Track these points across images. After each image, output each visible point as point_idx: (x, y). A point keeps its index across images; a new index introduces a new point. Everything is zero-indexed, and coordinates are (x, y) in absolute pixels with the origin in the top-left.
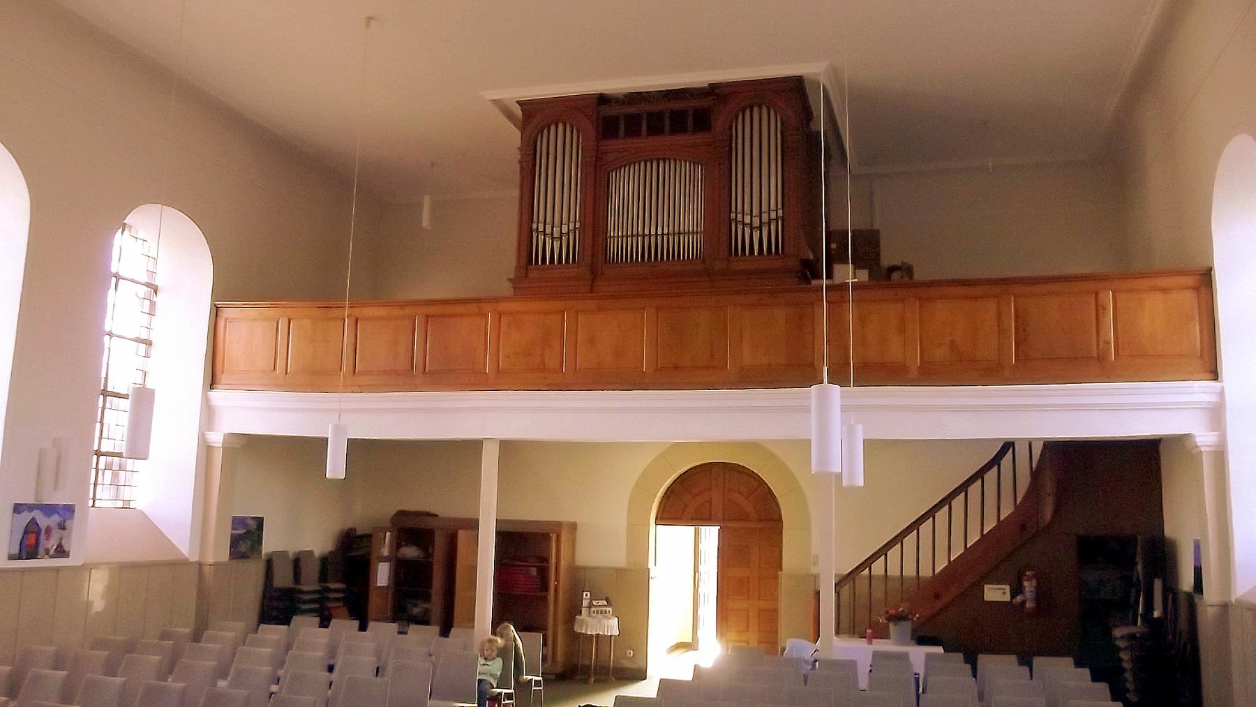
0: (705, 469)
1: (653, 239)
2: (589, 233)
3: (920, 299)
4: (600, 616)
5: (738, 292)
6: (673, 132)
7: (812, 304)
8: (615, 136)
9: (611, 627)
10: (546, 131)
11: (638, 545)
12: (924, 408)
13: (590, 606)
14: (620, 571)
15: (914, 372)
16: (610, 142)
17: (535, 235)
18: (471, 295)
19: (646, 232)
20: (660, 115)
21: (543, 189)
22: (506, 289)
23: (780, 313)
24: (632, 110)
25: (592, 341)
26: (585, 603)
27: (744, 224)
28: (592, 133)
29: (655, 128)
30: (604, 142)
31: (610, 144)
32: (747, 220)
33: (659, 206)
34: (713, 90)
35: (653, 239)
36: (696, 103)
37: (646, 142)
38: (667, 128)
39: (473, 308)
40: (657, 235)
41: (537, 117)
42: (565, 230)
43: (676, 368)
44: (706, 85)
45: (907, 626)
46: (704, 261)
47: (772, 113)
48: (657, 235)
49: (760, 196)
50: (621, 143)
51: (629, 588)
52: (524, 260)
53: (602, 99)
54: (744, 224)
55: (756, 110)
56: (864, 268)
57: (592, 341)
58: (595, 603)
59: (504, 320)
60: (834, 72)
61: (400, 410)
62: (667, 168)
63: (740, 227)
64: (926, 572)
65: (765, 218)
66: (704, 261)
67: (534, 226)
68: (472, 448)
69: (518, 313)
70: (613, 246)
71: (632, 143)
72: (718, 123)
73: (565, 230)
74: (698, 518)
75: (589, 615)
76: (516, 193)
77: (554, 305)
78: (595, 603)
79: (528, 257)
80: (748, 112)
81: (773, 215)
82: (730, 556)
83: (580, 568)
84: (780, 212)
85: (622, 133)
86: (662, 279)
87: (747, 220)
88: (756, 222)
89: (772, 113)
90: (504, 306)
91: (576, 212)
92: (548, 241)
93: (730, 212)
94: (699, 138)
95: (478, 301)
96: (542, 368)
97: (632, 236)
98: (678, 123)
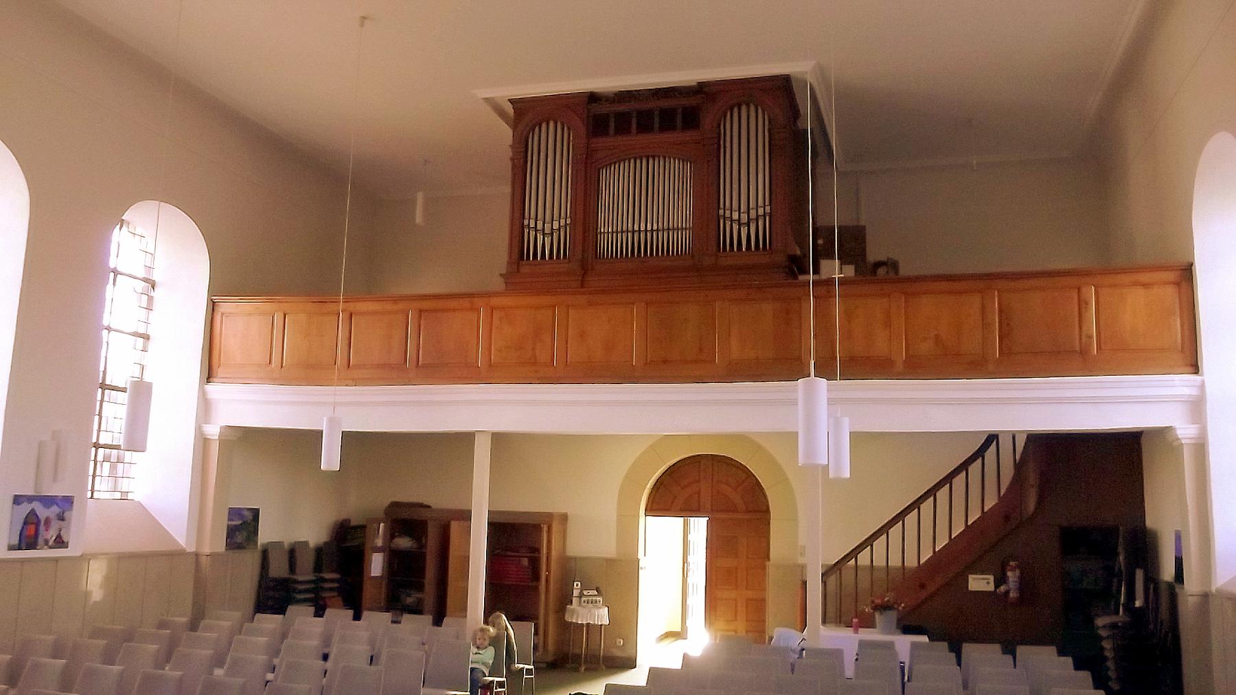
0: (694, 461)
1: (642, 235)
2: (580, 229)
3: (906, 294)
4: (590, 605)
5: (726, 287)
6: (662, 129)
7: (799, 299)
8: (605, 133)
9: (601, 616)
10: (537, 129)
11: (628, 536)
12: (909, 402)
13: (581, 596)
14: (610, 562)
15: (900, 366)
16: (600, 140)
17: (526, 231)
18: (464, 290)
19: (636, 228)
20: (650, 113)
21: (534, 186)
22: (498, 284)
23: (768, 308)
24: (621, 108)
25: (582, 335)
26: (576, 593)
27: (732, 221)
28: (582, 130)
29: (645, 126)
30: (594, 140)
31: (600, 142)
32: (735, 216)
33: (649, 202)
34: (702, 89)
35: (642, 235)
36: (685, 102)
37: (636, 140)
38: (657, 125)
39: (465, 303)
40: (646, 231)
41: (528, 115)
42: (556, 226)
43: (665, 362)
44: (694, 84)
45: (892, 616)
46: (693, 256)
47: (760, 111)
48: (646, 231)
49: (748, 193)
50: (611, 141)
51: (619, 578)
52: (516, 256)
53: (593, 97)
54: (732, 221)
55: (744, 108)
56: (850, 263)
57: (582, 335)
58: (585, 593)
59: (496, 314)
60: (821, 70)
61: (394, 403)
62: (656, 166)
63: (728, 223)
64: (911, 562)
65: (753, 214)
66: (693, 256)
67: (526, 222)
68: (464, 440)
69: (510, 307)
70: (603, 242)
71: (621, 140)
72: (707, 121)
73: (556, 226)
74: (687, 510)
75: (580, 604)
76: (507, 189)
77: (545, 300)
78: (585, 593)
79: (520, 253)
80: (736, 110)
81: (761, 211)
82: (719, 547)
83: (571, 558)
84: (768, 209)
85: (612, 131)
86: (651, 274)
87: (735, 216)
88: (744, 218)
89: (760, 111)
90: (496, 301)
91: (567, 208)
92: (540, 237)
93: (719, 208)
94: (688, 136)
95: (471, 295)
96: (534, 362)
97: (622, 232)
98: (668, 120)
